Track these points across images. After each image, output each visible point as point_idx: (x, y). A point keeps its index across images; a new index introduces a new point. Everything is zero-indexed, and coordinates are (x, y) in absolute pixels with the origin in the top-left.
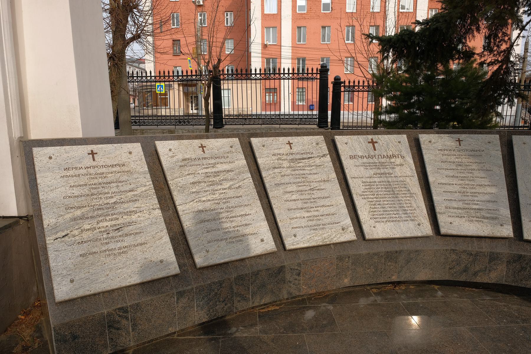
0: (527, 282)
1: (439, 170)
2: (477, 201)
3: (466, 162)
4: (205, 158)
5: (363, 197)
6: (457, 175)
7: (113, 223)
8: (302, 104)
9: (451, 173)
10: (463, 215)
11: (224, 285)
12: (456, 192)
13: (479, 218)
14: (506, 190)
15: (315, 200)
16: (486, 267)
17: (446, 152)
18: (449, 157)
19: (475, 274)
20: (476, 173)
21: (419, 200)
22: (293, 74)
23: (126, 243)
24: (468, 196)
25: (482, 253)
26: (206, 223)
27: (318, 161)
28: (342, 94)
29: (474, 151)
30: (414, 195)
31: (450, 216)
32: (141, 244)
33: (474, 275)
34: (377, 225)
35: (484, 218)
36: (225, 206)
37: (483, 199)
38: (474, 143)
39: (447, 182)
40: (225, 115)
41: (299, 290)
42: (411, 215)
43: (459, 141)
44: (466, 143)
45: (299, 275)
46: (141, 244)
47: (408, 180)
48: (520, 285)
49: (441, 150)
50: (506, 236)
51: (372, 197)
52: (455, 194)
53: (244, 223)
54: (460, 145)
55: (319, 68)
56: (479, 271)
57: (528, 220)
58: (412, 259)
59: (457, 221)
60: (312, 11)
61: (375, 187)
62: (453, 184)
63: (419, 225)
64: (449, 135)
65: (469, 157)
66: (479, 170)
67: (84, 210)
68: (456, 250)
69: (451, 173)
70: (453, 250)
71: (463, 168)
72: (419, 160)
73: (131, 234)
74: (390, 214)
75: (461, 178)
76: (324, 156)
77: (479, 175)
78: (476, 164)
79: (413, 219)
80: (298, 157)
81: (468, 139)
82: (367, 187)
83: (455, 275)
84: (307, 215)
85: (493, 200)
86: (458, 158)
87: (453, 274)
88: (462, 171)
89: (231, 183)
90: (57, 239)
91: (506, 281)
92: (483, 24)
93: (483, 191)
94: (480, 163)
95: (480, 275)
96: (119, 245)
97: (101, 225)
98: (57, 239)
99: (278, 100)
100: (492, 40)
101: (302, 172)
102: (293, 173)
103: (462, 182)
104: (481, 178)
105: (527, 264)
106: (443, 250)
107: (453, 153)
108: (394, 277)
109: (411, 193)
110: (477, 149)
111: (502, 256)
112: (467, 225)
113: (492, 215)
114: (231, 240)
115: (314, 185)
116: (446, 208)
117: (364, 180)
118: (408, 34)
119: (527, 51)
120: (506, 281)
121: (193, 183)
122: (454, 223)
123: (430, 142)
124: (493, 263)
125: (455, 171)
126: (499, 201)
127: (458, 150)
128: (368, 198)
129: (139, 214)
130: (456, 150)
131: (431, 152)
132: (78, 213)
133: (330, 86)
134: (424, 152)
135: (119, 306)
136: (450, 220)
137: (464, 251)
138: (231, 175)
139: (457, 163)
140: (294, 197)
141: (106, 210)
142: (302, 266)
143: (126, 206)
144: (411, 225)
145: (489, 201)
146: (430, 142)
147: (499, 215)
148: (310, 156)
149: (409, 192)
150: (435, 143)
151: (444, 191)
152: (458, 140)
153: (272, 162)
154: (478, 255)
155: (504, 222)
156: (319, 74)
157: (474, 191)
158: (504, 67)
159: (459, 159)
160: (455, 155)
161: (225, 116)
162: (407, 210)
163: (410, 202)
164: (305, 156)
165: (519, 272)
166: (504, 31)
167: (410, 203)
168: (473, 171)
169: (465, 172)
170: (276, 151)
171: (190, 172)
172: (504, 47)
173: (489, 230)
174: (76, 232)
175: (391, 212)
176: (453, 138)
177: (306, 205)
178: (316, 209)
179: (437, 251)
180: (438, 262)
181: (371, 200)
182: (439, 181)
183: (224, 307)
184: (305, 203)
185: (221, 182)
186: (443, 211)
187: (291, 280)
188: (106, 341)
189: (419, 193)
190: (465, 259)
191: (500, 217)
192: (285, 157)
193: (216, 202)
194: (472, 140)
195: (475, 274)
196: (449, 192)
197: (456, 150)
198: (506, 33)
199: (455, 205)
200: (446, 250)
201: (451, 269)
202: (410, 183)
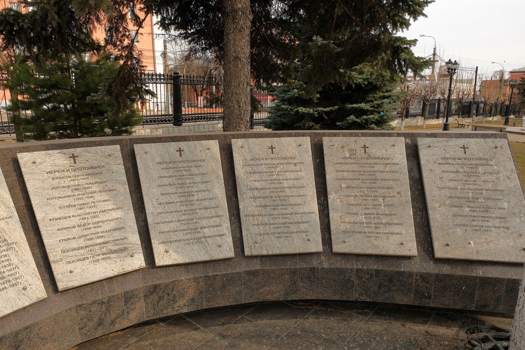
0: (167, 310)
1: (49, 201)
2: (102, 232)
3: (84, 184)
6: (73, 203)
9: (65, 202)
10: (86, 256)
12: (74, 227)
13: (105, 254)
14: (133, 211)
16: (123, 310)
17: (57, 174)
18: (62, 181)
19: (113, 323)
20: (98, 197)
21: (23, 251)
24: (90, 228)
25: (115, 296)
29: (93, 168)
30: (14, 246)
31: (70, 262)
33: (112, 324)
35: (112, 252)
37: (109, 228)
38: (92, 158)
39: (61, 216)
42: (10, 278)
43: (73, 157)
44: (82, 159)
49: (50, 172)
50: (138, 268)
52: (73, 229)
54: (75, 162)
56: (116, 318)
57: (158, 242)
58: (22, 341)
59: (78, 267)
62: (70, 217)
63: (24, 289)
64: (60, 151)
65: (87, 176)
66: (100, 192)
68: (83, 304)
69: (65, 202)
70: (80, 305)
71: (81, 193)
72: (21, 189)
75: (79, 207)
77: (101, 198)
78: (96, 185)
79: (14, 282)
81: (84, 153)
83: (89, 334)
85: (120, 227)
86: (73, 180)
87: (86, 334)
88: (81, 196)
91: (147, 317)
92: (103, 16)
93: (107, 219)
94: (101, 183)
95: (117, 322)
100: (114, 33)
103: (81, 211)
104: (104, 201)
105: (164, 292)
106: (66, 311)
107: (66, 174)
109: (8, 244)
110: (96, 165)
111: (138, 292)
112: (92, 267)
113: (120, 246)
116: (63, 251)
118: (13, 15)
119: (166, 48)
120: (147, 317)
122: (76, 270)
123: (34, 163)
124: (130, 303)
125: (71, 199)
126: (126, 226)
127: (73, 170)
130: (70, 170)
131: (36, 177)
134: (26, 178)
136: (70, 267)
137: (94, 302)
139: (73, 188)
144: (11, 292)
145: (115, 230)
146: (34, 163)
147: (128, 244)
149: (5, 243)
150: (41, 163)
151: (58, 230)
152: (71, 156)
154: (111, 301)
155: (134, 251)
157: (97, 220)
158: (129, 63)
159: (75, 182)
160: (70, 177)
162: (4, 272)
163: (8, 258)
165: (157, 303)
166: (125, 26)
167: (8, 260)
168: (93, 195)
169: (84, 197)
172: (126, 42)
173: (118, 267)
176: (65, 154)
179: (57, 316)
180: (62, 329)
182: (51, 215)
186: (59, 258)
189: (22, 241)
190: (96, 310)
191: (130, 246)
194: (89, 155)
196: (66, 228)
197: (70, 170)
198: (126, 28)
199: (74, 244)
200: (70, 309)
201: (82, 328)
202: (6, 228)
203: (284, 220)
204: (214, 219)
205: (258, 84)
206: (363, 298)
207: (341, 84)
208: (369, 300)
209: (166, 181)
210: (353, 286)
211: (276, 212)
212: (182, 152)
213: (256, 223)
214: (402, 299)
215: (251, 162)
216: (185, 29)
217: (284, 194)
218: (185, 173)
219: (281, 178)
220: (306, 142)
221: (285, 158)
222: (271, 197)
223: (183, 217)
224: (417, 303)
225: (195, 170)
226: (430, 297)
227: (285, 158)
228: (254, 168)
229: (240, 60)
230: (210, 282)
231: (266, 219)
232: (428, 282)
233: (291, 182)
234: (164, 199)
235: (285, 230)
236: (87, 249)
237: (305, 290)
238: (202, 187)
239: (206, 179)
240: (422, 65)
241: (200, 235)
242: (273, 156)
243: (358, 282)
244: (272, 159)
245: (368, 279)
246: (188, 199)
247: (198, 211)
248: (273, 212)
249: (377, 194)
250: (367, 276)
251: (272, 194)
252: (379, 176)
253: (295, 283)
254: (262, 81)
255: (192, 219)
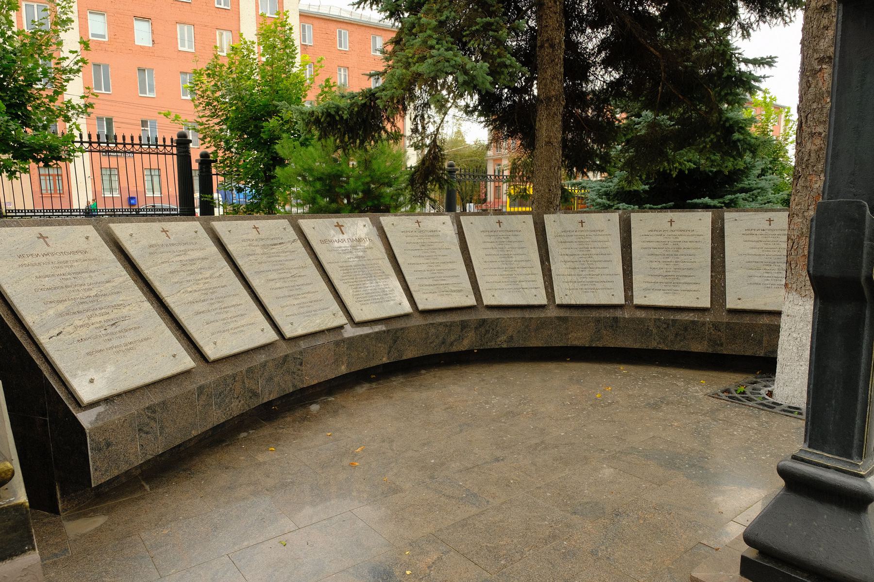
4: (173, 245)
5: (343, 281)
7: (106, 317)
8: (111, 195)
11: (237, 379)
12: (425, 271)
15: (299, 287)
17: (409, 234)
19: (452, 344)
22: (90, 143)
23: (129, 339)
26: (202, 315)
27: (290, 247)
28: (214, 177)
32: (146, 339)
34: (364, 307)
35: (452, 291)
36: (213, 296)
40: (6, 210)
41: (302, 382)
45: (301, 364)
46: (146, 339)
47: (380, 262)
48: (486, 347)
51: (352, 280)
53: (239, 313)
55: (175, 138)
56: (455, 341)
59: (430, 297)
60: (118, 40)
61: (352, 271)
67: (68, 303)
69: (417, 253)
73: (130, 330)
74: (373, 296)
76: (294, 241)
80: (269, 242)
82: (345, 272)
84: (296, 302)
86: (420, 239)
89: (211, 272)
90: (52, 337)
96: (123, 341)
97: (93, 320)
98: (52, 337)
99: (66, 188)
101: (278, 258)
102: (269, 259)
107: (414, 234)
108: (384, 359)
114: (233, 331)
115: (294, 272)
116: (420, 285)
117: (340, 264)
121: (172, 272)
128: (349, 282)
129: (128, 308)
132: (61, 307)
133: (195, 166)
135: (147, 405)
136: (425, 296)
138: (205, 264)
140: (278, 285)
141: (91, 305)
142: (304, 354)
143: (110, 298)
146: (393, 224)
148: (281, 241)
153: (244, 248)
156: (175, 146)
157: (439, 268)
160: (417, 236)
161: (6, 213)
164: (276, 242)
170: (245, 237)
171: (163, 260)
174: (70, 329)
175: (373, 294)
177: (292, 293)
178: (303, 296)
181: (351, 284)
183: (238, 405)
184: (291, 290)
185: (200, 271)
187: (295, 370)
188: (137, 448)
192: (255, 243)
193: (203, 292)
195: (452, 344)
199: (426, 282)
203: (590, 280)
204: (530, 276)
205: (571, 173)
206: (661, 347)
207: (671, 170)
208: (666, 349)
209: (489, 245)
210: (651, 335)
211: (584, 273)
212: (501, 224)
213: (566, 280)
214: (698, 347)
215: (562, 234)
216: (488, 116)
217: (592, 259)
218: (504, 240)
219: (590, 246)
220: (615, 217)
221: (594, 231)
222: (580, 261)
223: (505, 273)
224: (711, 350)
225: (512, 238)
226: (722, 345)
227: (594, 231)
228: (565, 238)
229: (552, 144)
230: (526, 324)
231: (575, 278)
232: (720, 331)
233: (598, 249)
234: (488, 259)
235: (592, 287)
236: (435, 286)
237: (608, 338)
238: (520, 251)
239: (523, 246)
240: (759, 145)
241: (518, 287)
242: (582, 229)
243: (656, 331)
244: (581, 231)
245: (665, 329)
246: (508, 259)
247: (516, 269)
248: (581, 273)
249: (678, 260)
250: (665, 326)
251: (581, 259)
252: (682, 245)
253: (599, 330)
254: (575, 169)
255: (511, 275)
